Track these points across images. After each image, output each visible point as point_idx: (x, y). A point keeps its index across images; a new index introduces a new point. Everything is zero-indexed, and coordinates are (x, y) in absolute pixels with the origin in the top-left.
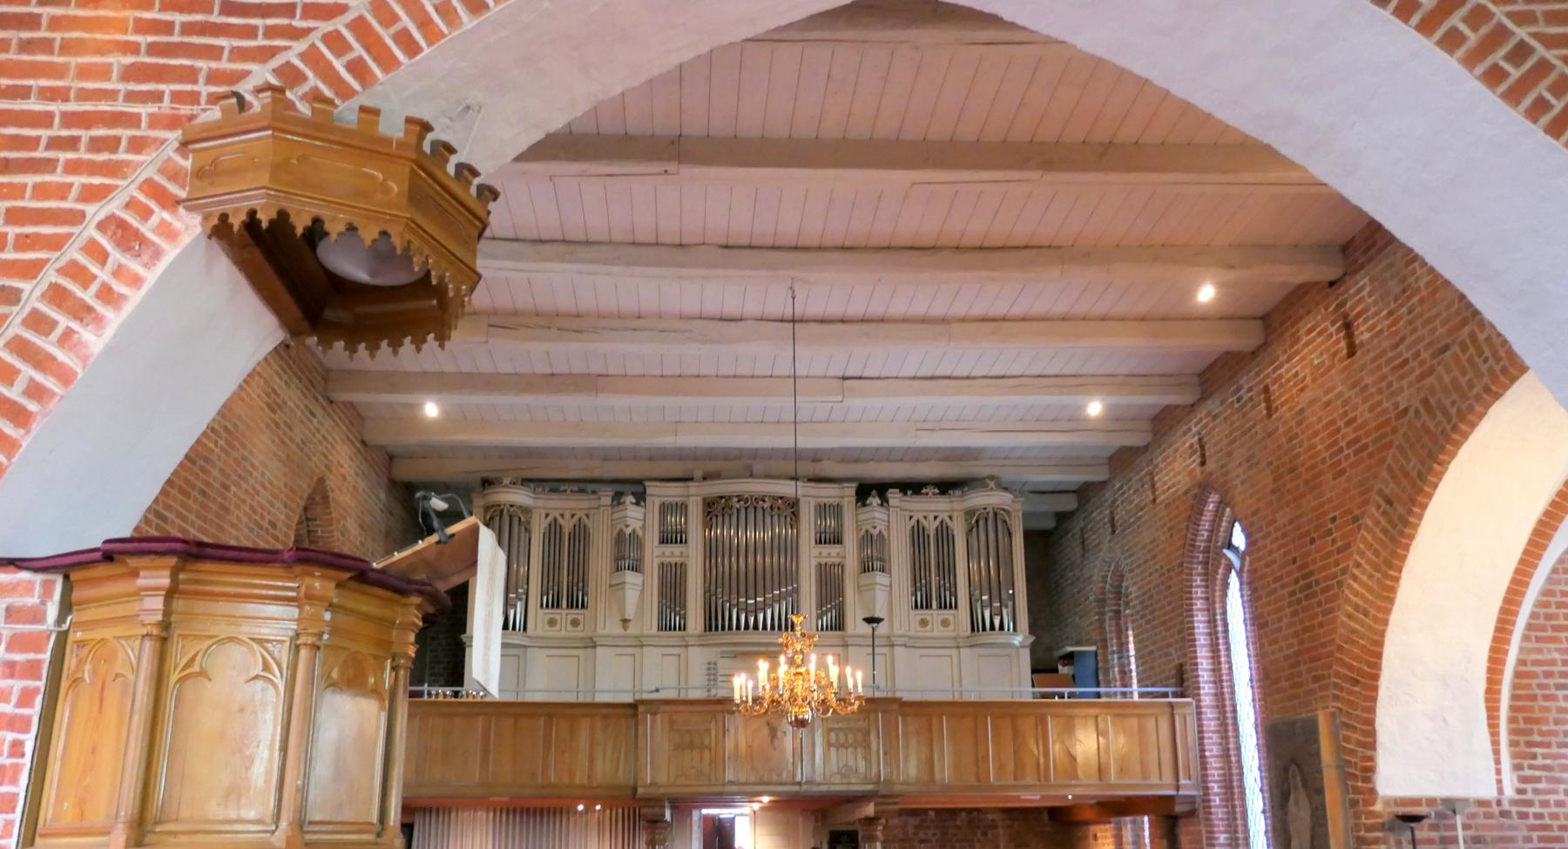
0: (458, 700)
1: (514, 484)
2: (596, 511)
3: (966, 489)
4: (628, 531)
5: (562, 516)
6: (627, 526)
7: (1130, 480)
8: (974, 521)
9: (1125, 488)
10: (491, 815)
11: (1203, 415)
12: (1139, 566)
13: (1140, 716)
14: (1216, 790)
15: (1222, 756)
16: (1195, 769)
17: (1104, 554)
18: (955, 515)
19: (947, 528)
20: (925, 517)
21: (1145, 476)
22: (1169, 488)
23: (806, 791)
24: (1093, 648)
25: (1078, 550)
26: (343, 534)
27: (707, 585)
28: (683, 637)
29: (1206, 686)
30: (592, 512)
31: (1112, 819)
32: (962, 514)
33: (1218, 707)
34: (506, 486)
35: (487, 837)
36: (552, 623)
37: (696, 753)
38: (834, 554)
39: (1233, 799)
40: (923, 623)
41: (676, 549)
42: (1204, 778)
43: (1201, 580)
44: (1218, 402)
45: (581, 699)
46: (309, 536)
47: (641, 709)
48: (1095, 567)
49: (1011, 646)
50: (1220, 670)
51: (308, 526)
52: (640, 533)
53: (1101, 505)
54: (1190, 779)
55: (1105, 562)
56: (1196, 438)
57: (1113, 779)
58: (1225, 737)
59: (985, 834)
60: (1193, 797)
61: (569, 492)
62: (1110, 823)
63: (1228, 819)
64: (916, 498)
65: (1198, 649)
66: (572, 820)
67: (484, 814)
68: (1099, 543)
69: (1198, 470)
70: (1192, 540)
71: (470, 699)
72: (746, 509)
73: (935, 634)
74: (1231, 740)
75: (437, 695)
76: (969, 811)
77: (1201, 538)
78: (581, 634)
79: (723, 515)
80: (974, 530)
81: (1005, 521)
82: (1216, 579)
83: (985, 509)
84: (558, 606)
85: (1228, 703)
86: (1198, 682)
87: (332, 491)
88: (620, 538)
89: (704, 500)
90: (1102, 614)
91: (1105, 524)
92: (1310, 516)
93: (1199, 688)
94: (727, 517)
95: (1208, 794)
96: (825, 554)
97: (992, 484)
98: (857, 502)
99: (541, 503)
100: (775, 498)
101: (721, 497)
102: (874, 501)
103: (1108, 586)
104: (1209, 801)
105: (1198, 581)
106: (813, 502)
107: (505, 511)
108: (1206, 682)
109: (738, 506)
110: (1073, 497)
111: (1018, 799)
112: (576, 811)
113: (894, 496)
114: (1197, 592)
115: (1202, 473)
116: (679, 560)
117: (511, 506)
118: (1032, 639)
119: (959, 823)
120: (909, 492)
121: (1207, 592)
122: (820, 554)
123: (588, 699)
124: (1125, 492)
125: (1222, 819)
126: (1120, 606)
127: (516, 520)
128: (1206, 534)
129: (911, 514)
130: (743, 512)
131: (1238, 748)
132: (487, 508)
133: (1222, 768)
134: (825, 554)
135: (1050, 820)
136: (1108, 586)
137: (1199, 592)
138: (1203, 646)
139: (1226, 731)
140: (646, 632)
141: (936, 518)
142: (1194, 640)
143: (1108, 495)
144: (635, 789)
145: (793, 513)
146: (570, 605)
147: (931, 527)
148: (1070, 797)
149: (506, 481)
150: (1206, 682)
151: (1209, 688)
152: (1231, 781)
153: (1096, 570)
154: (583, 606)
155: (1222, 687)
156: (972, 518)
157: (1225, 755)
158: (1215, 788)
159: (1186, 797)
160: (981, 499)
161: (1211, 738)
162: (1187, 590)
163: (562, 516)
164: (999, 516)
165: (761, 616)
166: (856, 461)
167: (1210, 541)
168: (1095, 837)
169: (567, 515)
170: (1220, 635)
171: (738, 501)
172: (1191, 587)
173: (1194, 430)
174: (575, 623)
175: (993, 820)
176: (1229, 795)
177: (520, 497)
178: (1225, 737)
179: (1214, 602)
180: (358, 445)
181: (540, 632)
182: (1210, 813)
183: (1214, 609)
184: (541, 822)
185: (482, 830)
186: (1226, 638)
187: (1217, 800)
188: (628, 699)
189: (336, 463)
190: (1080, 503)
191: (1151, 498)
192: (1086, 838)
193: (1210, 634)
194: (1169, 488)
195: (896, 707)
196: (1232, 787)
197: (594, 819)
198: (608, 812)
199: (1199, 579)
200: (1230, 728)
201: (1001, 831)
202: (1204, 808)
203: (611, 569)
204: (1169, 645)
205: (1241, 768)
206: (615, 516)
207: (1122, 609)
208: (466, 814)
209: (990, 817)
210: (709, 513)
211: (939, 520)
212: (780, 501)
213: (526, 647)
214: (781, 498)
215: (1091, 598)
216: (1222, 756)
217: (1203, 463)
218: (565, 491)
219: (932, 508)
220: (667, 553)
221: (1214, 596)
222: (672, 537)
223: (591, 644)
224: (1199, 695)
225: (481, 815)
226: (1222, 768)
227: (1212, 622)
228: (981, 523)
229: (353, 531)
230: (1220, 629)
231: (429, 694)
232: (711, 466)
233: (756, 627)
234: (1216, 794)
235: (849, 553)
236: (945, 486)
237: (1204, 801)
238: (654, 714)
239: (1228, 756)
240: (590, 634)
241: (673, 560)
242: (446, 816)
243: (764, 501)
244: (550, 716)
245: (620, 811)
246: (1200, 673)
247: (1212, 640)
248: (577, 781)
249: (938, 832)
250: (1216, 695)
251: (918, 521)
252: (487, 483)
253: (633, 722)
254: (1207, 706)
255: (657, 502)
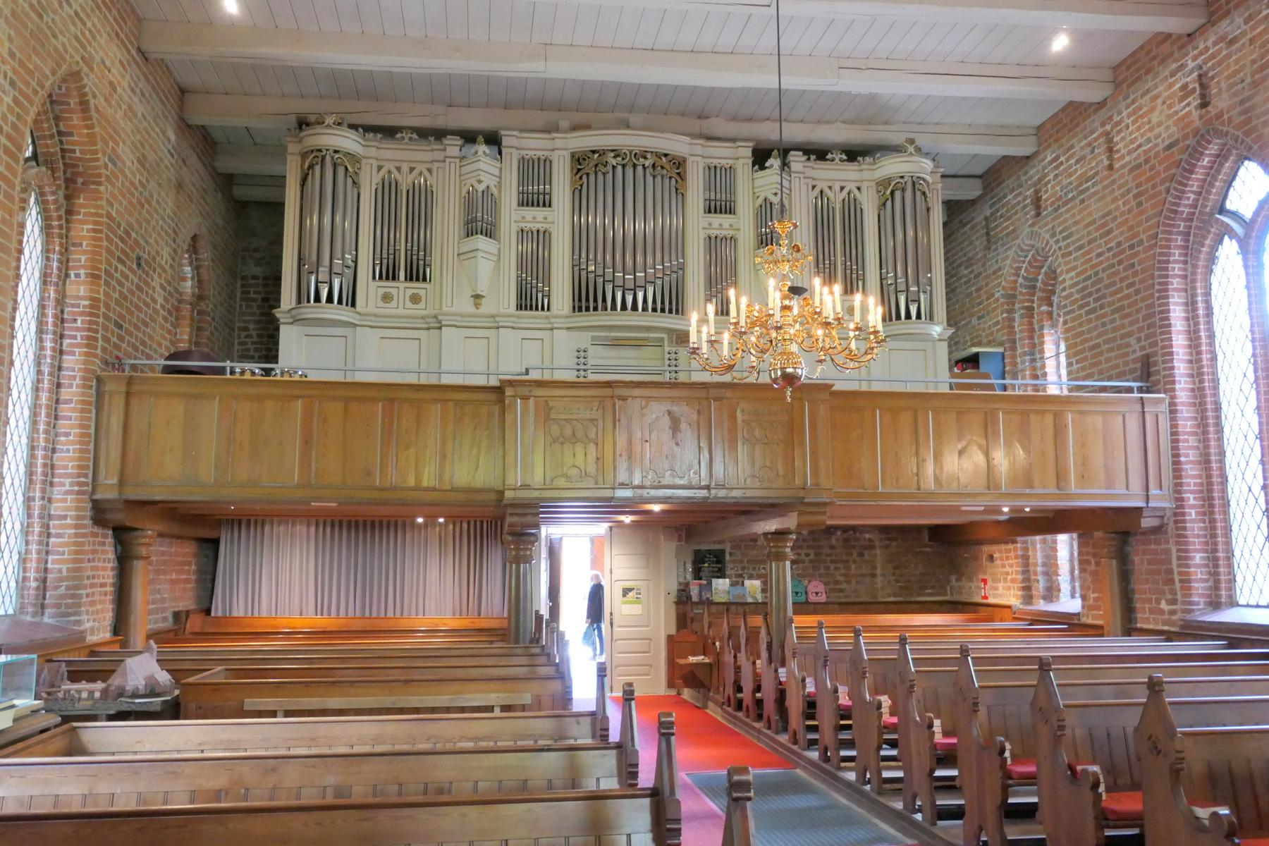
0: (271, 378)
1: (339, 124)
2: (441, 165)
3: (878, 155)
4: (481, 188)
5: (398, 169)
6: (480, 182)
7: (1072, 147)
8: (888, 192)
9: (1062, 159)
10: (313, 529)
11: (1209, 43)
12: (1080, 248)
13: (1103, 413)
14: (1192, 502)
15: (1199, 463)
16: (1167, 479)
17: (1024, 239)
18: (864, 186)
19: (855, 200)
20: (830, 188)
21: (1099, 137)
22: (1140, 146)
23: (716, 497)
24: (1001, 350)
25: (979, 244)
26: (111, 160)
27: (576, 257)
28: (547, 317)
29: (1183, 380)
30: (436, 165)
31: (1019, 539)
32: (873, 184)
33: (1195, 405)
34: (329, 126)
35: (308, 547)
36: (387, 298)
37: (579, 448)
38: (726, 225)
39: (1212, 513)
40: (387, 298)
41: (540, 213)
42: (1178, 488)
43: (1180, 255)
44: (1239, 20)
45: (424, 380)
46: (63, 157)
47: (509, 392)
48: (1007, 257)
49: (927, 338)
50: (1200, 360)
51: (61, 143)
52: (495, 191)
53: (1020, 186)
54: (1161, 489)
55: (1022, 250)
56: (1195, 74)
57: (1073, 488)
58: (1205, 440)
59: (861, 555)
60: (1164, 509)
61: (406, 140)
62: (1015, 542)
63: (1205, 536)
64: (821, 164)
65: (1174, 337)
66: (408, 535)
67: (305, 529)
68: (1014, 231)
69: (1195, 114)
70: (1174, 204)
71: (286, 378)
72: (624, 166)
73: (401, 311)
74: (1212, 443)
75: (243, 373)
76: (845, 529)
77: (1187, 202)
78: (424, 312)
79: (596, 173)
80: (889, 203)
81: (924, 193)
82: (1200, 252)
83: (902, 177)
84: (394, 279)
85: (1209, 399)
86: (1173, 376)
87: (95, 97)
88: (469, 203)
89: (573, 155)
90: (1011, 311)
91: (1025, 207)
92: (1140, 248)
93: (1174, 382)
94: (600, 177)
95: (1182, 507)
96: (716, 225)
97: (911, 149)
98: (753, 166)
99: (373, 152)
100: (658, 155)
101: (594, 152)
102: (774, 162)
103: (1020, 280)
104: (1183, 514)
105: (1176, 254)
106: (702, 163)
107: (328, 158)
108: (1181, 376)
109: (614, 162)
110: (978, 182)
111: (956, 510)
112: (414, 525)
113: (796, 159)
114: (1174, 269)
115: (1201, 117)
116: (541, 227)
117: (336, 152)
118: (951, 331)
119: (834, 542)
120: (813, 157)
121: (1185, 270)
122: (710, 224)
123: (433, 380)
124: (1062, 163)
125: (1198, 536)
126: (1033, 302)
127: (341, 170)
128: (1192, 196)
129: (814, 183)
130: (619, 168)
131: (1222, 453)
132: (304, 156)
133: (1200, 477)
134: (716, 225)
135: (930, 540)
136: (1020, 280)
137: (1176, 269)
138: (1179, 332)
139: (1205, 433)
140: (502, 311)
141: (842, 188)
142: (1169, 325)
143: (1033, 172)
144: (502, 493)
145: (678, 174)
146: (410, 278)
147: (837, 199)
148: (1006, 509)
149: (329, 120)
150: (1181, 376)
151: (1186, 382)
152: (1210, 491)
153: (1008, 262)
154: (424, 279)
155: (1201, 381)
156: (886, 189)
157: (1205, 461)
158: (1191, 499)
159: (1155, 509)
160: (891, 167)
161: (1187, 441)
162: (1164, 266)
163: (398, 169)
164: (917, 186)
165: (640, 295)
166: (750, 119)
167: (1195, 207)
168: (991, 558)
169: (405, 168)
170: (1201, 320)
171: (615, 157)
172: (1168, 262)
173: (1191, 64)
174: (415, 299)
175: (870, 540)
176: (1206, 509)
177: (348, 141)
178: (1205, 440)
179: (1194, 281)
180: (134, 52)
181: (371, 309)
182: (1185, 529)
183: (1194, 288)
184: (373, 536)
185: (301, 545)
186: (1209, 323)
187: (1192, 514)
188: (494, 382)
189: (98, 59)
190: (985, 188)
191: (1106, 162)
192: (976, 558)
193: (1187, 319)
194: (1140, 146)
195: (825, 396)
196: (1212, 498)
197: (434, 534)
198: (451, 526)
199: (1177, 252)
200: (1211, 429)
201: (878, 551)
202: (1176, 522)
203: (459, 235)
204: (1129, 335)
205: (1224, 477)
206: (464, 170)
207: (1035, 305)
208: (282, 528)
209: (867, 536)
210: (579, 170)
211: (846, 191)
212: (664, 159)
213: (355, 325)
214: (666, 155)
215: (997, 295)
216: (1199, 463)
217: (1204, 105)
218: (403, 138)
219: (838, 174)
220: (529, 218)
221: (1194, 273)
222: (536, 199)
223: (437, 324)
224: (1173, 390)
225: (301, 529)
226: (1200, 477)
227: (1191, 305)
228: (898, 194)
229: (129, 164)
230: (1201, 312)
231: (232, 373)
232: (580, 117)
233: (635, 307)
234: (1192, 507)
235: (743, 224)
236: (853, 154)
237: (1175, 514)
238: (525, 398)
239: (1208, 462)
240: (434, 312)
241: (535, 226)
242: (259, 530)
243: (645, 158)
244: (391, 401)
245: (465, 525)
246: (1176, 364)
247: (1189, 326)
248: (425, 484)
249: (812, 552)
250: (1193, 390)
251: (822, 192)
252: (303, 123)
253: (496, 409)
254: (1183, 404)
255: (516, 155)
